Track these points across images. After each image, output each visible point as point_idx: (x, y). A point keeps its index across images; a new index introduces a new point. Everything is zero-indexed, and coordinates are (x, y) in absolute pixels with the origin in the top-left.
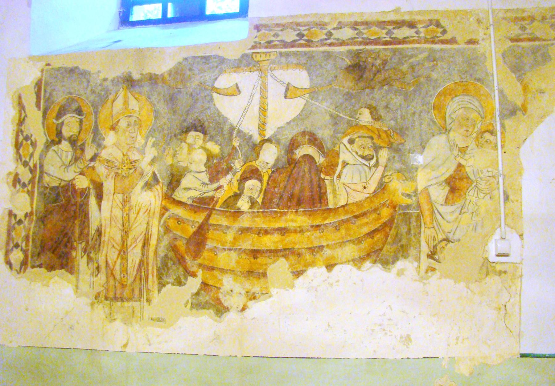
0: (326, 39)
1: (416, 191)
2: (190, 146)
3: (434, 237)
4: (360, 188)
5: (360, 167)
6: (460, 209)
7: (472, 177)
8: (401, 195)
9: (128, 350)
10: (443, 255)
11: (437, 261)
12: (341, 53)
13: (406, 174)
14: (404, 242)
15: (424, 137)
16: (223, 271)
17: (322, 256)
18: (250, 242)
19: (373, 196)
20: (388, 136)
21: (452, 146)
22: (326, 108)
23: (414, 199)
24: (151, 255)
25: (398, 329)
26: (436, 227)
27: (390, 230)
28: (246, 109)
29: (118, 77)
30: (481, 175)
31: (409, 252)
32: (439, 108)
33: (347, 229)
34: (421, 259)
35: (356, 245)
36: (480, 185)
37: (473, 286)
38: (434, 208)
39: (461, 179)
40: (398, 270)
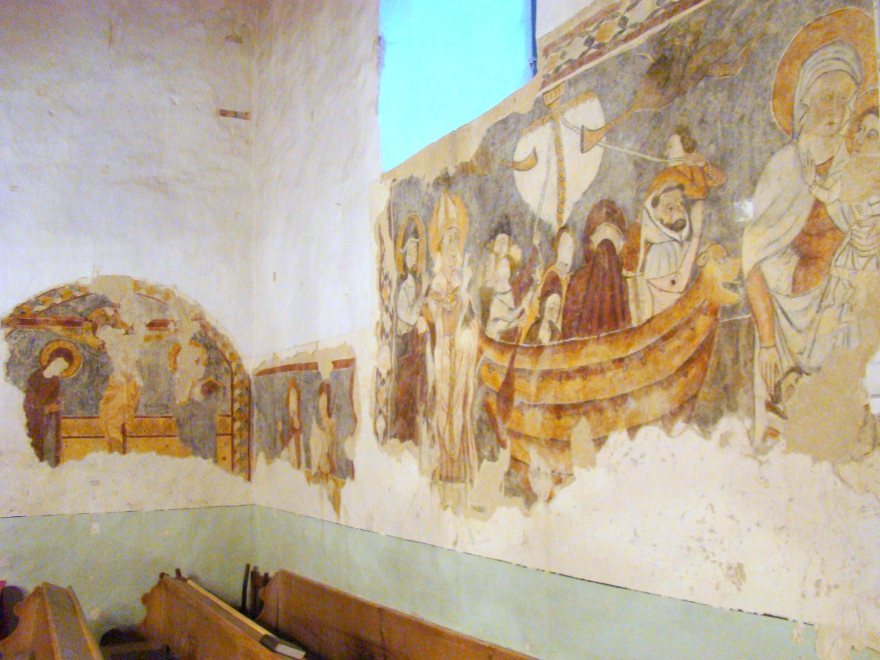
0: (621, 32)
1: (740, 276)
2: (497, 255)
3: (776, 366)
4: (666, 284)
5: (668, 245)
6: (818, 300)
7: (843, 226)
8: (721, 287)
9: (458, 549)
10: (790, 402)
11: (782, 415)
12: (638, 49)
13: (727, 244)
14: (728, 380)
15: (757, 163)
16: (529, 438)
17: (624, 412)
18: (552, 393)
19: (685, 296)
20: (705, 176)
21: (804, 164)
22: (629, 152)
23: (741, 290)
24: (468, 417)
25: (724, 550)
26: (779, 345)
27: (709, 357)
28: (545, 184)
29: (437, 179)
30: (859, 217)
31: (738, 399)
32: (782, 92)
33: (656, 362)
34: (757, 414)
35: (665, 389)
36: (857, 239)
37: (847, 470)
38: (776, 305)
39: (821, 235)
40: (722, 436)
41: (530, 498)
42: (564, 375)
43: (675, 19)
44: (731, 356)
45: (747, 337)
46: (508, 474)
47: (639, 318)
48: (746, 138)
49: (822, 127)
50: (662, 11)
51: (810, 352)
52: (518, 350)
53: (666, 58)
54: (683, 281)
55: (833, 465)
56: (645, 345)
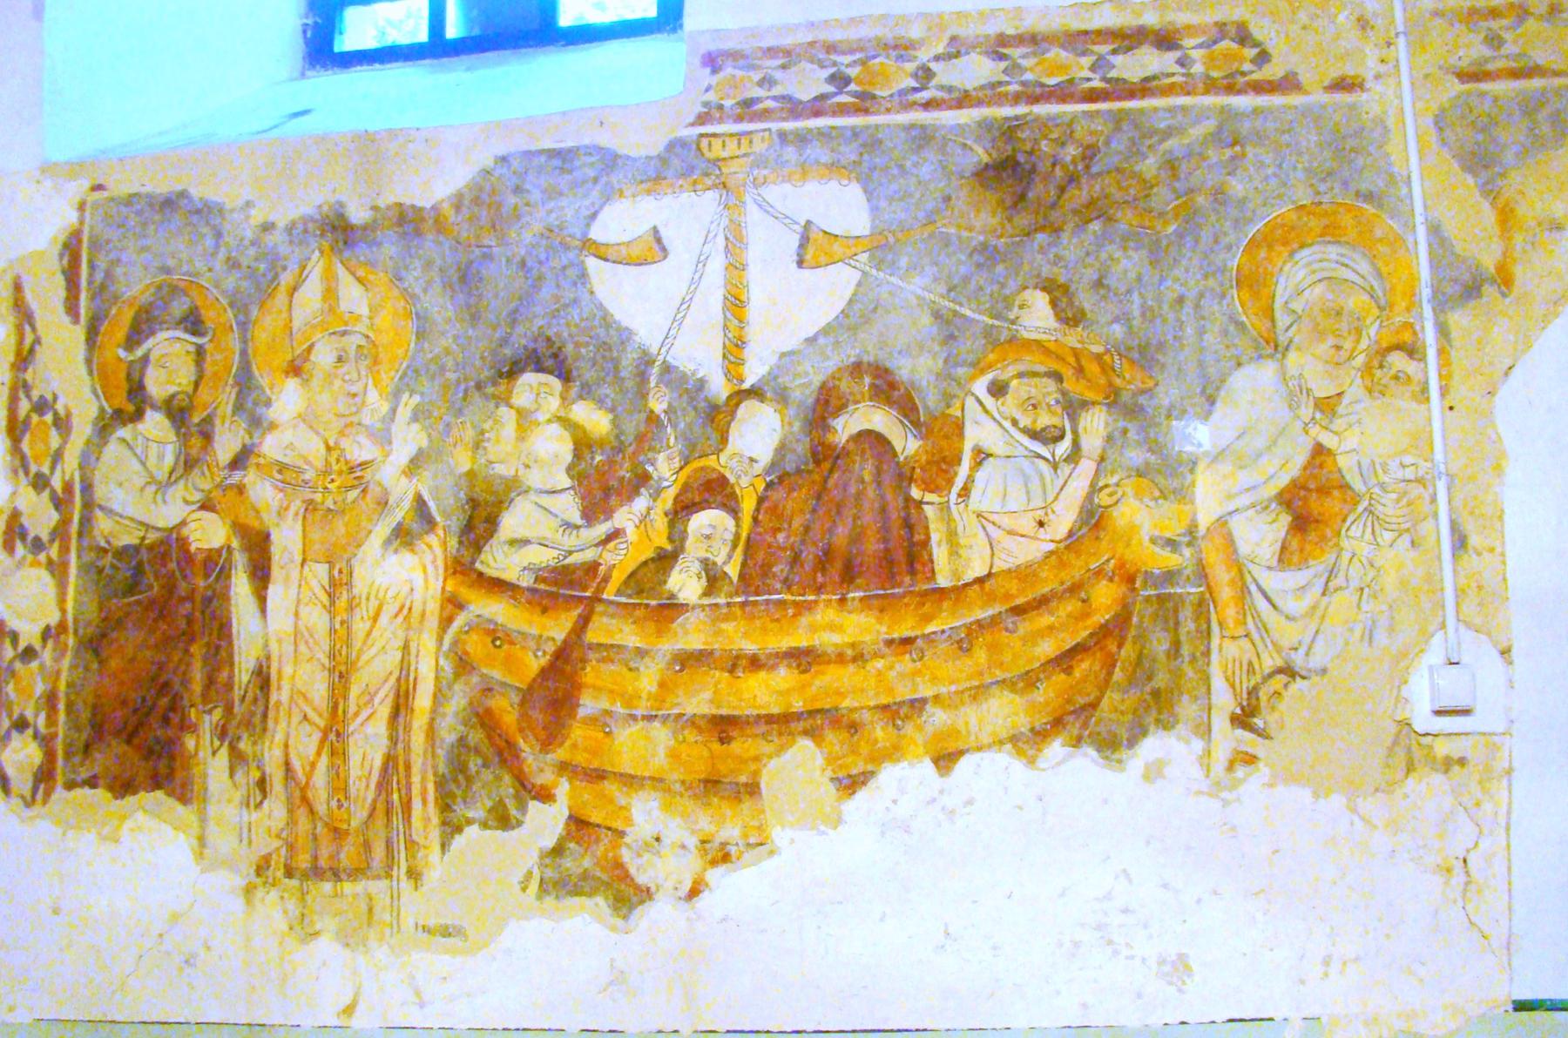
0: (915, 90)
1: (1191, 531)
2: (524, 416)
3: (1250, 663)
4: (1026, 524)
5: (1025, 464)
6: (1323, 580)
7: (1357, 484)
8: (1147, 543)
12: (961, 128)
14: (1161, 680)
17: (920, 728)
18: (707, 695)
19: (1067, 547)
20: (1106, 369)
21: (1295, 392)
22: (919, 291)
23: (1187, 552)
24: (418, 740)
26: (1255, 635)
27: (1120, 646)
28: (686, 303)
30: (1383, 478)
31: (1178, 710)
32: (1253, 282)
35: (1022, 692)
36: (1380, 508)
39: (1324, 491)
40: (1147, 766)
41: (626, 894)
42: (744, 662)
43: (1044, 109)
44: (1165, 646)
45: (1197, 619)
46: (558, 851)
47: (955, 574)
48: (1189, 331)
49: (1324, 347)
50: (1015, 88)
51: (1309, 649)
52: (599, 608)
53: (1017, 164)
54: (1064, 520)
55: (1349, 800)
56: (969, 620)
